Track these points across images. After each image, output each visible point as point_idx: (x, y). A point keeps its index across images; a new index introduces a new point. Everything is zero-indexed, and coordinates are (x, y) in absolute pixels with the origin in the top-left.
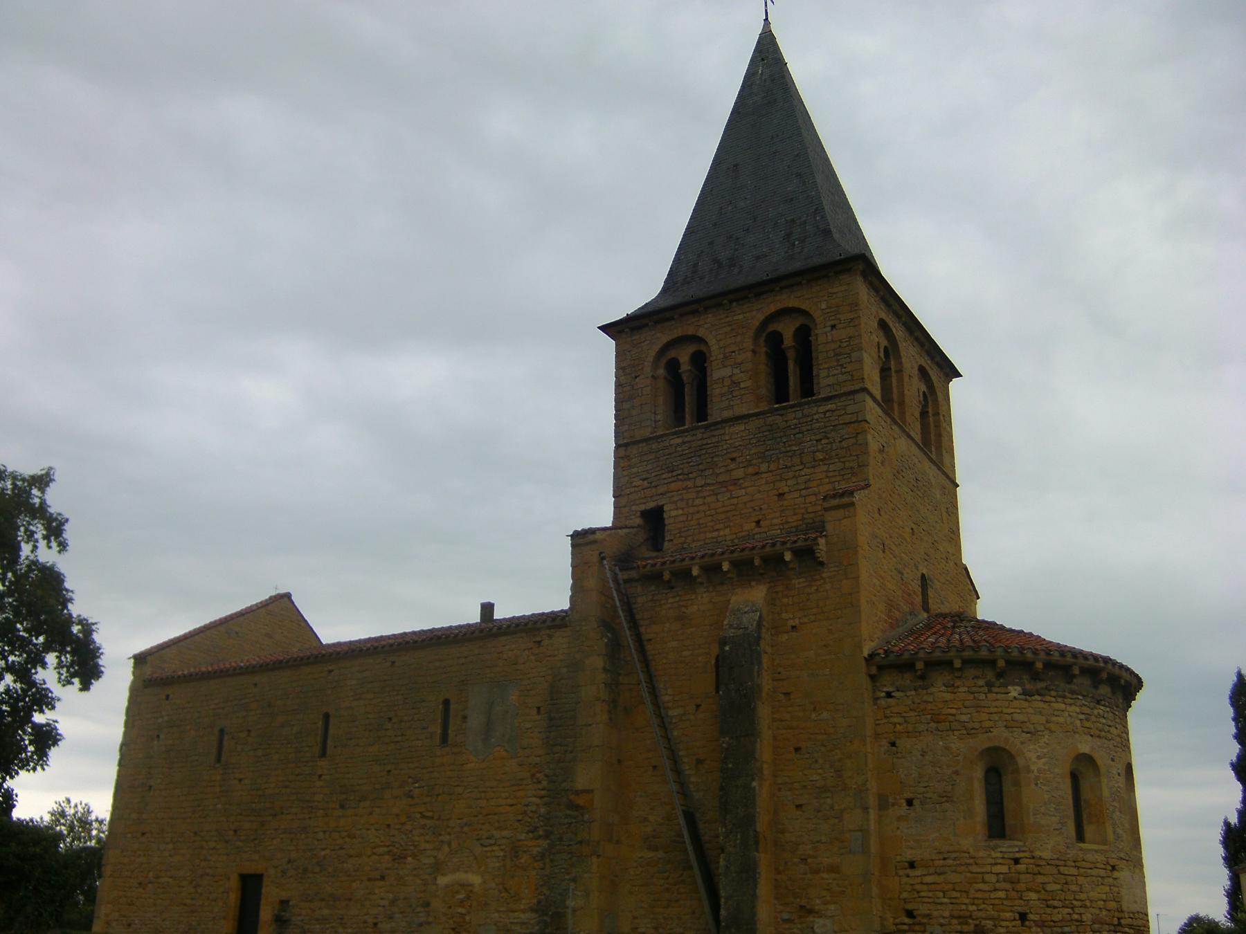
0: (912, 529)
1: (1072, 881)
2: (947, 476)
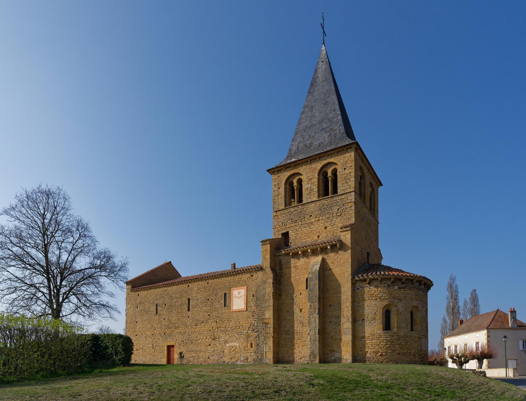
2: (375, 219)
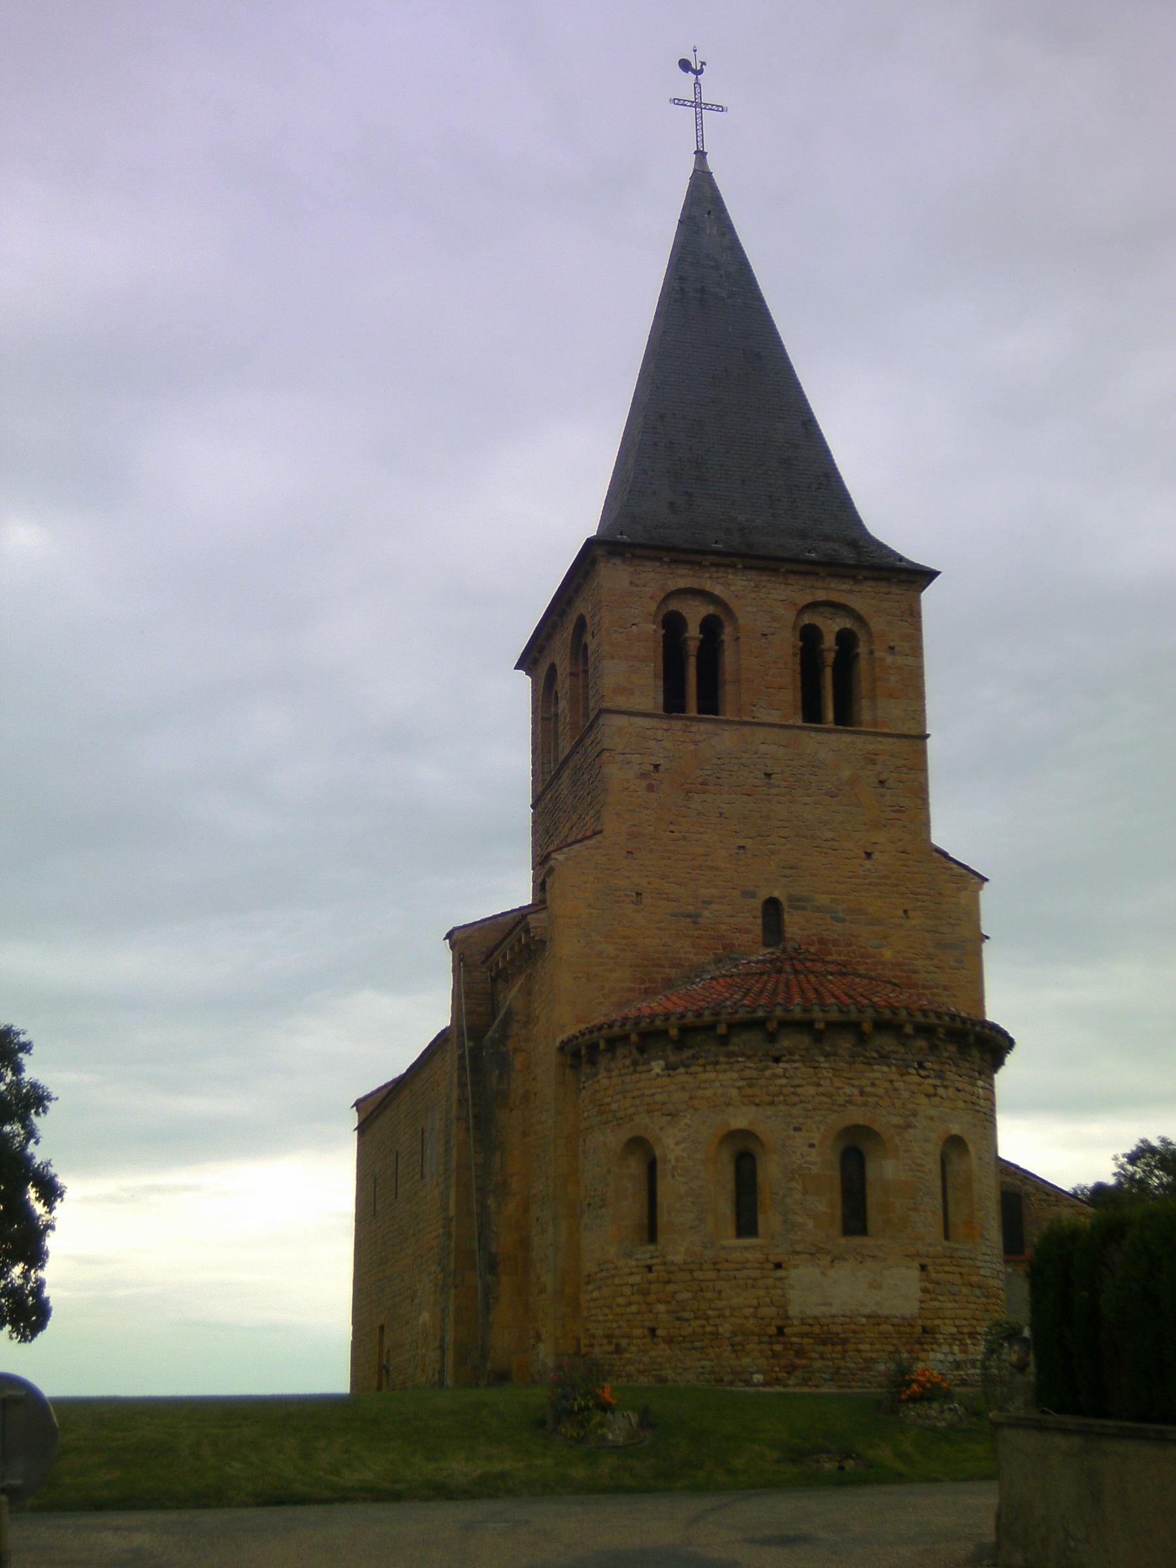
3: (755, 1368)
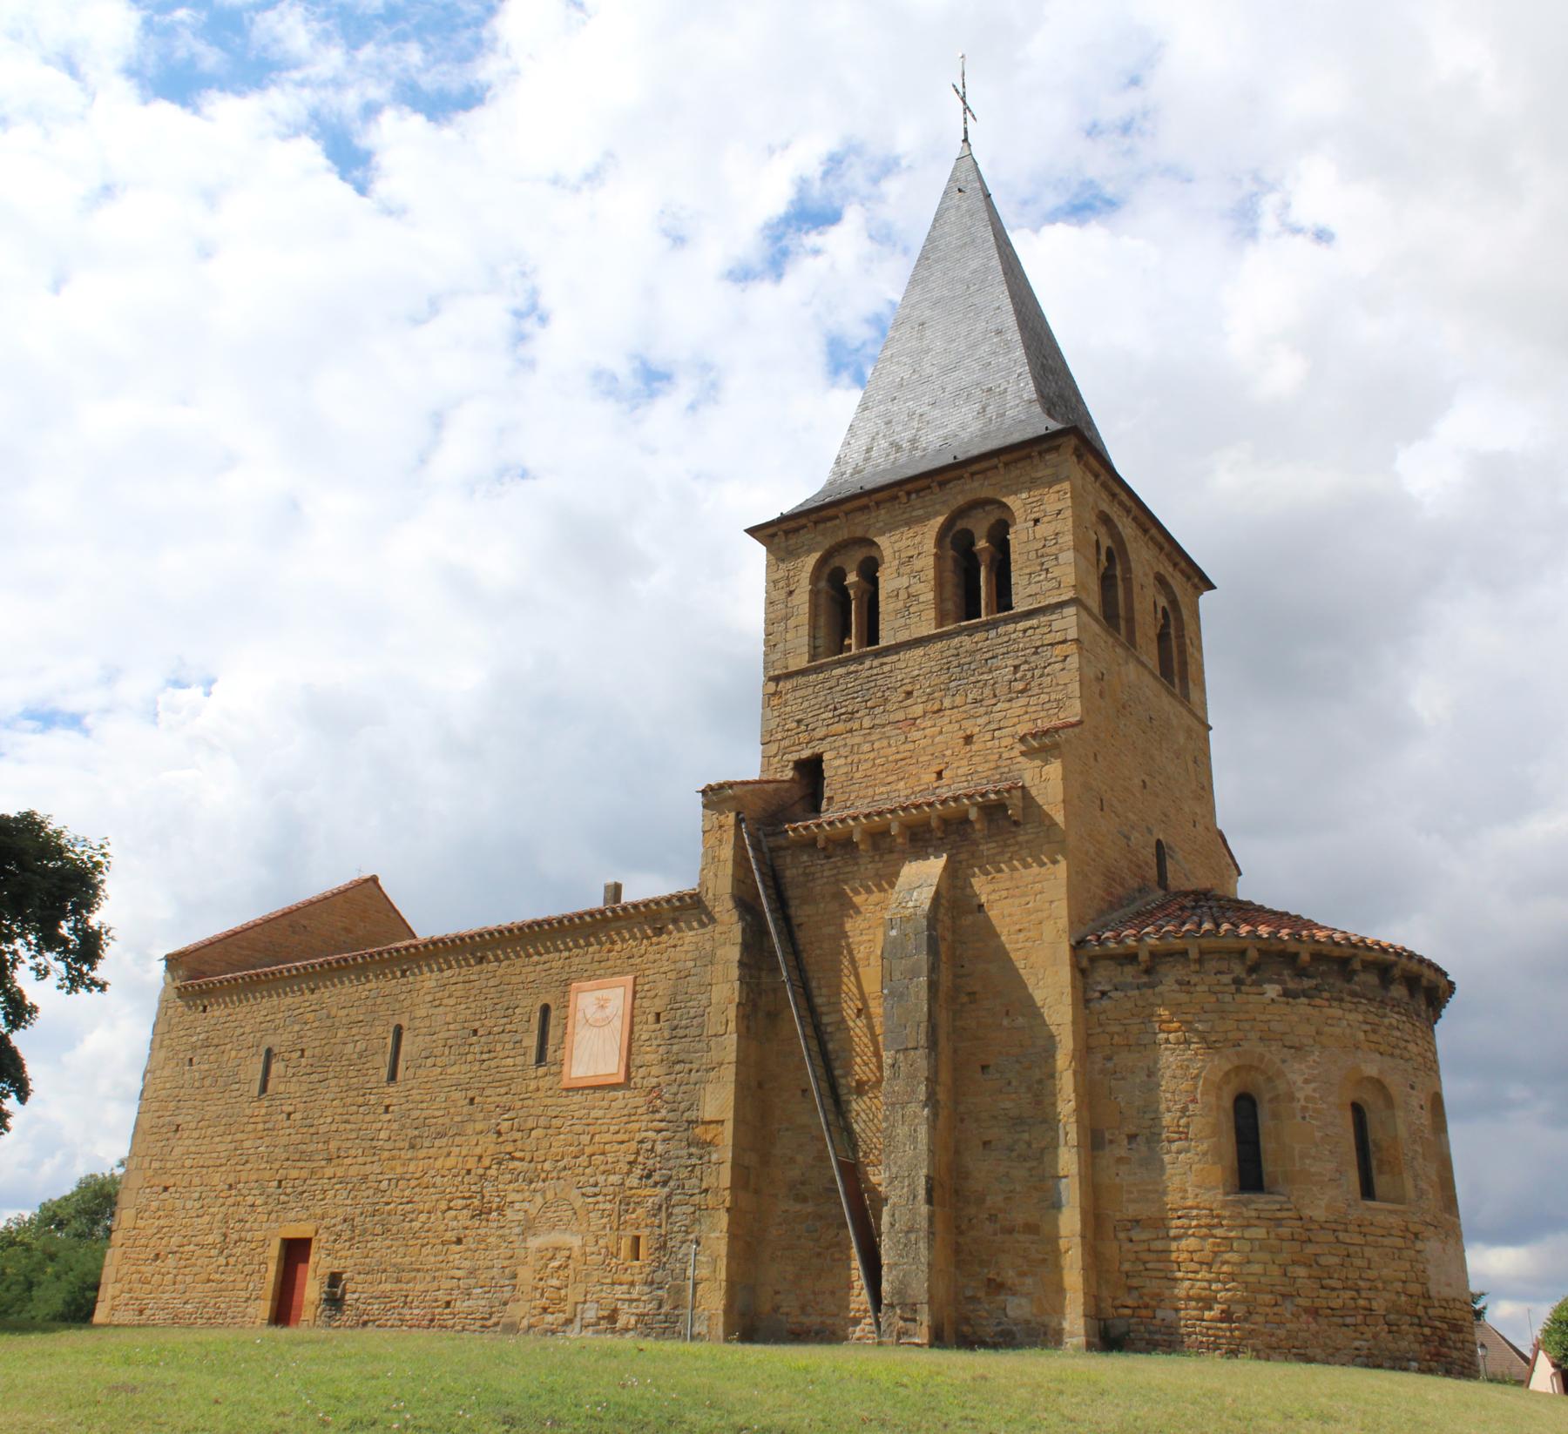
0: (1143, 781)
1: (1356, 1252)
2: (1194, 715)
3: (1411, 1354)
